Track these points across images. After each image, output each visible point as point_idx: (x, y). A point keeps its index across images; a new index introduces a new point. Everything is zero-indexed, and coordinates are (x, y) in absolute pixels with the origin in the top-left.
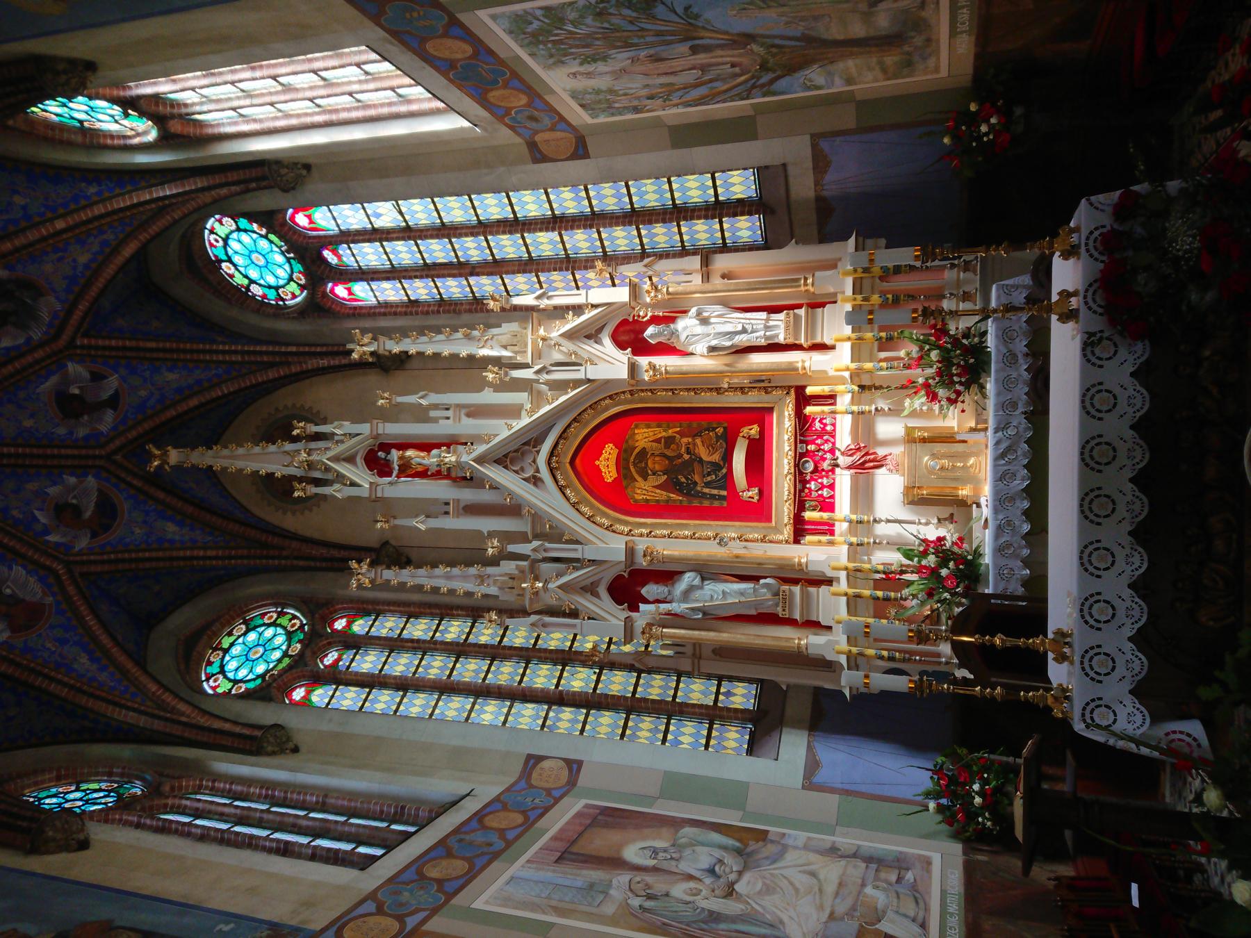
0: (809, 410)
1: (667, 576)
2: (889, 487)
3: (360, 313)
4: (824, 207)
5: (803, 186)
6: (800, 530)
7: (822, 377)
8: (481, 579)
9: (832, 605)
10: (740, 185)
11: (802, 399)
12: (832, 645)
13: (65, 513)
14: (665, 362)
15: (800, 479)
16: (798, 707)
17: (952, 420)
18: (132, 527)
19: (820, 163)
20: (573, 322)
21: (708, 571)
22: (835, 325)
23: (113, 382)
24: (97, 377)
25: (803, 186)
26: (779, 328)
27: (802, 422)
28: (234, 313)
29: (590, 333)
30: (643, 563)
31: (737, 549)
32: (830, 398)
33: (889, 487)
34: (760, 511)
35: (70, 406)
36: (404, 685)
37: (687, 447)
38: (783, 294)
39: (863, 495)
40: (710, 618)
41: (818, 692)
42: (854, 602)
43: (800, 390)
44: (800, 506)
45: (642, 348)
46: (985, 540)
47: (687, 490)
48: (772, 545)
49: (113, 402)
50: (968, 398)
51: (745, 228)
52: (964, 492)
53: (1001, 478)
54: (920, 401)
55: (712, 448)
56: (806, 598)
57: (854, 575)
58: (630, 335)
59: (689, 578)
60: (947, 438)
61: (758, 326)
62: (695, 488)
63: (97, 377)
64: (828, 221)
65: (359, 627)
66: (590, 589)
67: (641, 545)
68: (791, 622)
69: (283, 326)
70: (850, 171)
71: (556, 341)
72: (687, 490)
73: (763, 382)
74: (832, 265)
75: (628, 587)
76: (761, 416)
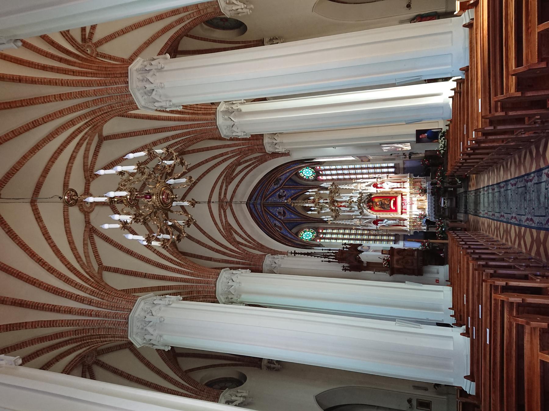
0: (523, 228)
1: (382, 220)
2: (415, 207)
3: (323, 180)
4: (404, 168)
5: (401, 166)
6: (402, 213)
7: (405, 192)
8: (351, 222)
9: (407, 223)
10: (392, 165)
11: (402, 195)
12: (408, 228)
13: (279, 213)
14: (382, 190)
15: (402, 206)
16: (402, 238)
17: (423, 198)
18: (288, 215)
19: (404, 163)
20: (367, 184)
21: (389, 219)
22: (407, 185)
23: (285, 193)
24: (284, 192)
25: (401, 166)
26: (398, 185)
27: (402, 198)
28: (301, 181)
29: (369, 185)
30: (379, 218)
31: (393, 216)
32: (406, 195)
33: (415, 207)
34: (396, 210)
35: (280, 197)
36: (336, 239)
37: (386, 202)
38: (399, 181)
39: (411, 208)
40: (389, 225)
41: (404, 235)
42: (410, 222)
43: (402, 194)
44: (402, 210)
45: (377, 188)
46: (427, 213)
47: (384, 208)
48: (398, 215)
49: (285, 196)
50: (425, 195)
51: (392, 170)
52: (424, 207)
53: (429, 205)
54: (419, 196)
55: (387, 202)
56: (403, 223)
57: (410, 218)
58: (375, 186)
59: (386, 220)
60: (422, 200)
61: (396, 185)
62: (385, 208)
63: (284, 192)
64: (405, 171)
65: (324, 231)
66: (370, 222)
67: (378, 216)
68: (401, 226)
69: (309, 183)
70: (408, 164)
71: (365, 186)
72: (384, 208)
73: (396, 192)
74: (406, 177)
75: (376, 222)
76: (396, 197)
